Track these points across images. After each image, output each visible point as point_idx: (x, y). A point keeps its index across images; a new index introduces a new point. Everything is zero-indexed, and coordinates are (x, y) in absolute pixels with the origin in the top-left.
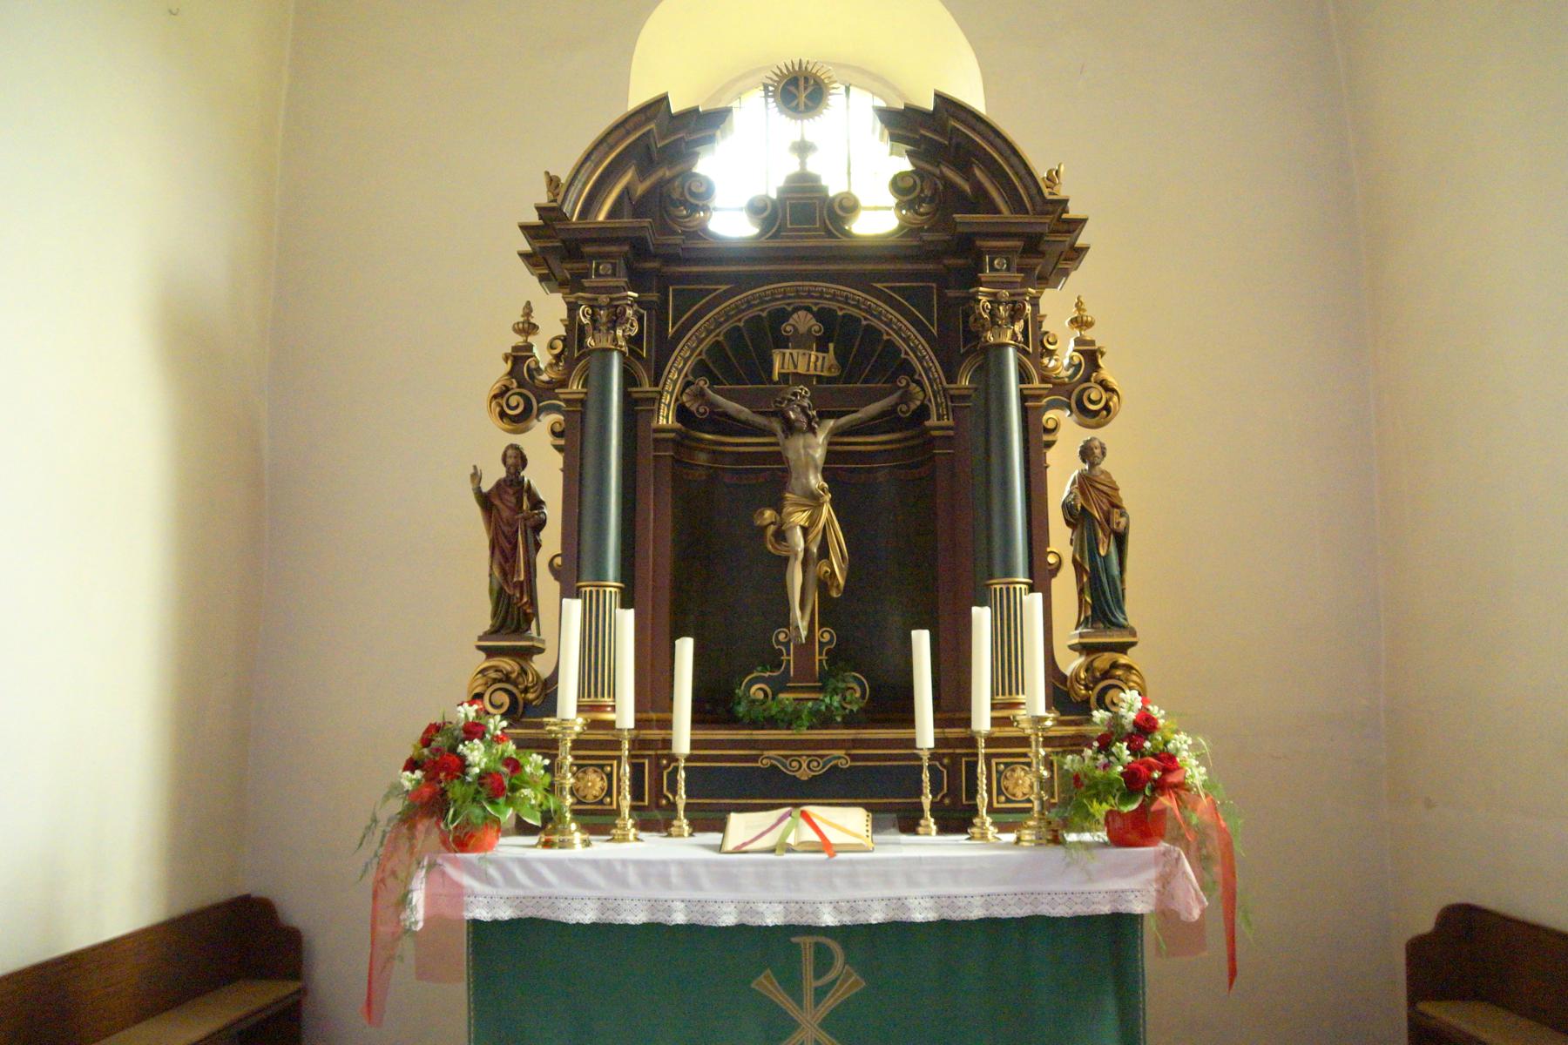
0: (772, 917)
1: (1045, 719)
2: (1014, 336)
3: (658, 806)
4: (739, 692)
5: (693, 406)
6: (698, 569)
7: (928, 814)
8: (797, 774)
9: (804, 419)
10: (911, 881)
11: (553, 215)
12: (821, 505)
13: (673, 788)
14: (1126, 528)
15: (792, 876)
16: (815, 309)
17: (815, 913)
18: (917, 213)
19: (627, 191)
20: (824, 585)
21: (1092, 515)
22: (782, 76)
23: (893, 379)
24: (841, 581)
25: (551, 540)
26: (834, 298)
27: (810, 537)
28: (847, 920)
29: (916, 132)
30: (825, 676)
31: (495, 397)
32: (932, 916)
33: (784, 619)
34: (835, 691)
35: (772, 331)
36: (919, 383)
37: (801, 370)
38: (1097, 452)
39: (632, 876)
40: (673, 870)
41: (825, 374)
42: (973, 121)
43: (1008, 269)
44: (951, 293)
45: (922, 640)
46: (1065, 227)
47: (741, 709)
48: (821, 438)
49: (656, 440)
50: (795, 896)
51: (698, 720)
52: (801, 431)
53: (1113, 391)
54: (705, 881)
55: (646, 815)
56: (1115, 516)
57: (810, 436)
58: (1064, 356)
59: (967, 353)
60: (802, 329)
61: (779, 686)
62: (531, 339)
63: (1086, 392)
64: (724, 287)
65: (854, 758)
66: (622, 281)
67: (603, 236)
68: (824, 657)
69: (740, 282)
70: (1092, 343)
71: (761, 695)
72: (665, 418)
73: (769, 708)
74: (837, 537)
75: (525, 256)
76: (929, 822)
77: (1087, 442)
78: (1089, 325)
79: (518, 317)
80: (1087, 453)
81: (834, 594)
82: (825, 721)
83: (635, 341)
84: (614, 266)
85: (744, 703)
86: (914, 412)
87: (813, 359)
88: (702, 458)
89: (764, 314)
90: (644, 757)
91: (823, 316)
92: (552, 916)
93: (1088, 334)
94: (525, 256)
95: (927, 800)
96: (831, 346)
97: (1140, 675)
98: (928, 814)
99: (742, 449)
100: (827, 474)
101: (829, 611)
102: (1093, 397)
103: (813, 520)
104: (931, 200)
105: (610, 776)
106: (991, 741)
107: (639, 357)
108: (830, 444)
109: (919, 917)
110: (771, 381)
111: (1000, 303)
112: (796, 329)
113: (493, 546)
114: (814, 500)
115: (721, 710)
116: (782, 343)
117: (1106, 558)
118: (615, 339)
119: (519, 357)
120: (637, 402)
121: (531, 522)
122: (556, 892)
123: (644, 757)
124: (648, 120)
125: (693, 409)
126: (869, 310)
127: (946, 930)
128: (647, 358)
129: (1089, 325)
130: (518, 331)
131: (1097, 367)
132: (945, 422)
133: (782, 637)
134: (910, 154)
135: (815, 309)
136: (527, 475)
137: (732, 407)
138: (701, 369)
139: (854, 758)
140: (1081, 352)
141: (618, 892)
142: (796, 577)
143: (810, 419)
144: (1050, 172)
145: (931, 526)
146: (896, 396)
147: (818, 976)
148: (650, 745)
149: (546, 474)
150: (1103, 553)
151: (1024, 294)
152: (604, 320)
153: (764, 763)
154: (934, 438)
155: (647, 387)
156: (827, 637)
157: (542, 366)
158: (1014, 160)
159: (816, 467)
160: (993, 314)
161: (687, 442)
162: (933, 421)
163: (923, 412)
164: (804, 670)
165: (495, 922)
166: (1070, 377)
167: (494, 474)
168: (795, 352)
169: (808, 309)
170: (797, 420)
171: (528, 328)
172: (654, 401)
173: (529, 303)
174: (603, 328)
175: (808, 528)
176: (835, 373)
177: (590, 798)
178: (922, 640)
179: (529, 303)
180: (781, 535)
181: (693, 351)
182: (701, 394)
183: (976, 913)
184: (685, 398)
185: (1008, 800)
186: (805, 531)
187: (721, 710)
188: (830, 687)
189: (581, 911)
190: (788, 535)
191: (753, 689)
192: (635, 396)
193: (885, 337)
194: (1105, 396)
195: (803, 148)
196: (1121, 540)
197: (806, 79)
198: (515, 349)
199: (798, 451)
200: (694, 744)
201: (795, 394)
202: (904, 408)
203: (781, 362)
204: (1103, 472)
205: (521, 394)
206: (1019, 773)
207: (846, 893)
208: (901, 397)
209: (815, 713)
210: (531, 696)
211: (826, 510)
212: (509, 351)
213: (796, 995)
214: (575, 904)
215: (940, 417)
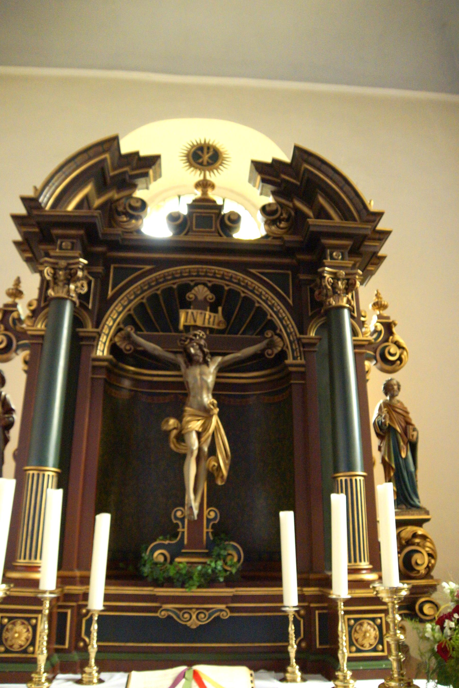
1: (401, 589)
2: (348, 301)
3: (77, 648)
4: (146, 555)
5: (123, 345)
7: (293, 661)
8: (188, 624)
9: (201, 354)
11: (33, 204)
12: (211, 416)
13: (88, 633)
14: (417, 438)
16: (209, 284)
18: (278, 227)
19: (86, 198)
20: (211, 476)
21: (395, 430)
23: (262, 333)
24: (225, 472)
26: (223, 278)
27: (203, 439)
29: (278, 176)
30: (210, 545)
33: (181, 501)
34: (219, 557)
35: (179, 297)
36: (280, 336)
37: (199, 323)
38: (396, 387)
41: (215, 327)
42: (319, 163)
43: (343, 259)
44: (302, 277)
45: (287, 519)
46: (377, 236)
47: (146, 570)
48: (212, 368)
49: (94, 367)
51: (114, 574)
52: (198, 363)
55: (66, 657)
56: (410, 432)
57: (204, 367)
58: (372, 323)
59: (313, 317)
60: (200, 298)
61: (176, 552)
62: (17, 300)
63: (383, 351)
65: (232, 610)
66: (77, 253)
67: (68, 222)
68: (210, 530)
69: (160, 264)
70: (388, 318)
71: (161, 559)
72: (102, 350)
73: (168, 570)
74: (223, 440)
75: (17, 244)
76: (294, 669)
78: (384, 307)
79: (10, 285)
80: (389, 389)
82: (210, 581)
83: (84, 298)
84: (73, 243)
85: (148, 566)
86: (276, 355)
87: (207, 317)
88: (127, 383)
89: (175, 286)
90: (68, 607)
91: (215, 289)
93: (385, 313)
94: (17, 244)
95: (292, 650)
96: (220, 309)
97: (431, 542)
98: (293, 661)
99: (155, 379)
101: (215, 495)
102: (392, 351)
103: (205, 427)
104: (287, 220)
105: (35, 628)
106: (347, 602)
107: (86, 309)
108: (217, 377)
110: (176, 329)
111: (339, 279)
112: (196, 297)
114: (206, 413)
115: (131, 568)
116: (186, 305)
117: (406, 459)
118: (69, 291)
120: (82, 338)
121: (3, 423)
123: (68, 607)
124: (104, 152)
125: (122, 347)
126: (246, 287)
128: (90, 311)
129: (384, 307)
130: (10, 294)
131: (391, 333)
132: (299, 361)
133: (179, 514)
134: (274, 193)
135: (209, 284)
137: (150, 346)
138: (129, 320)
139: (232, 610)
140: (382, 323)
142: (192, 469)
143: (205, 354)
145: (294, 431)
148: (71, 599)
150: (403, 455)
151: (356, 274)
152: (62, 278)
153: (162, 614)
154: (291, 373)
155: (90, 328)
156: (212, 515)
157: (23, 317)
158: (347, 188)
159: (208, 389)
160: (334, 286)
161: (116, 371)
162: (290, 361)
163: (282, 355)
164: (195, 539)
166: (376, 339)
168: (195, 312)
169: (205, 284)
170: (196, 355)
171: (16, 293)
172: (95, 339)
174: (61, 284)
175: (201, 432)
176: (222, 327)
177: (16, 647)
178: (287, 519)
180: (181, 437)
181: (124, 307)
182: (128, 337)
184: (116, 339)
185: (358, 651)
186: (199, 435)
187: (131, 568)
188: (215, 553)
190: (186, 437)
191: (156, 554)
192: (82, 334)
193: (257, 305)
194: (398, 352)
195: (204, 185)
196: (413, 447)
198: (6, 305)
199: (195, 377)
200: (107, 597)
201: (195, 335)
202: (270, 351)
203: (184, 318)
204: (398, 401)
206: (366, 627)
208: (268, 344)
209: (203, 575)
211: (215, 420)
215: (295, 358)
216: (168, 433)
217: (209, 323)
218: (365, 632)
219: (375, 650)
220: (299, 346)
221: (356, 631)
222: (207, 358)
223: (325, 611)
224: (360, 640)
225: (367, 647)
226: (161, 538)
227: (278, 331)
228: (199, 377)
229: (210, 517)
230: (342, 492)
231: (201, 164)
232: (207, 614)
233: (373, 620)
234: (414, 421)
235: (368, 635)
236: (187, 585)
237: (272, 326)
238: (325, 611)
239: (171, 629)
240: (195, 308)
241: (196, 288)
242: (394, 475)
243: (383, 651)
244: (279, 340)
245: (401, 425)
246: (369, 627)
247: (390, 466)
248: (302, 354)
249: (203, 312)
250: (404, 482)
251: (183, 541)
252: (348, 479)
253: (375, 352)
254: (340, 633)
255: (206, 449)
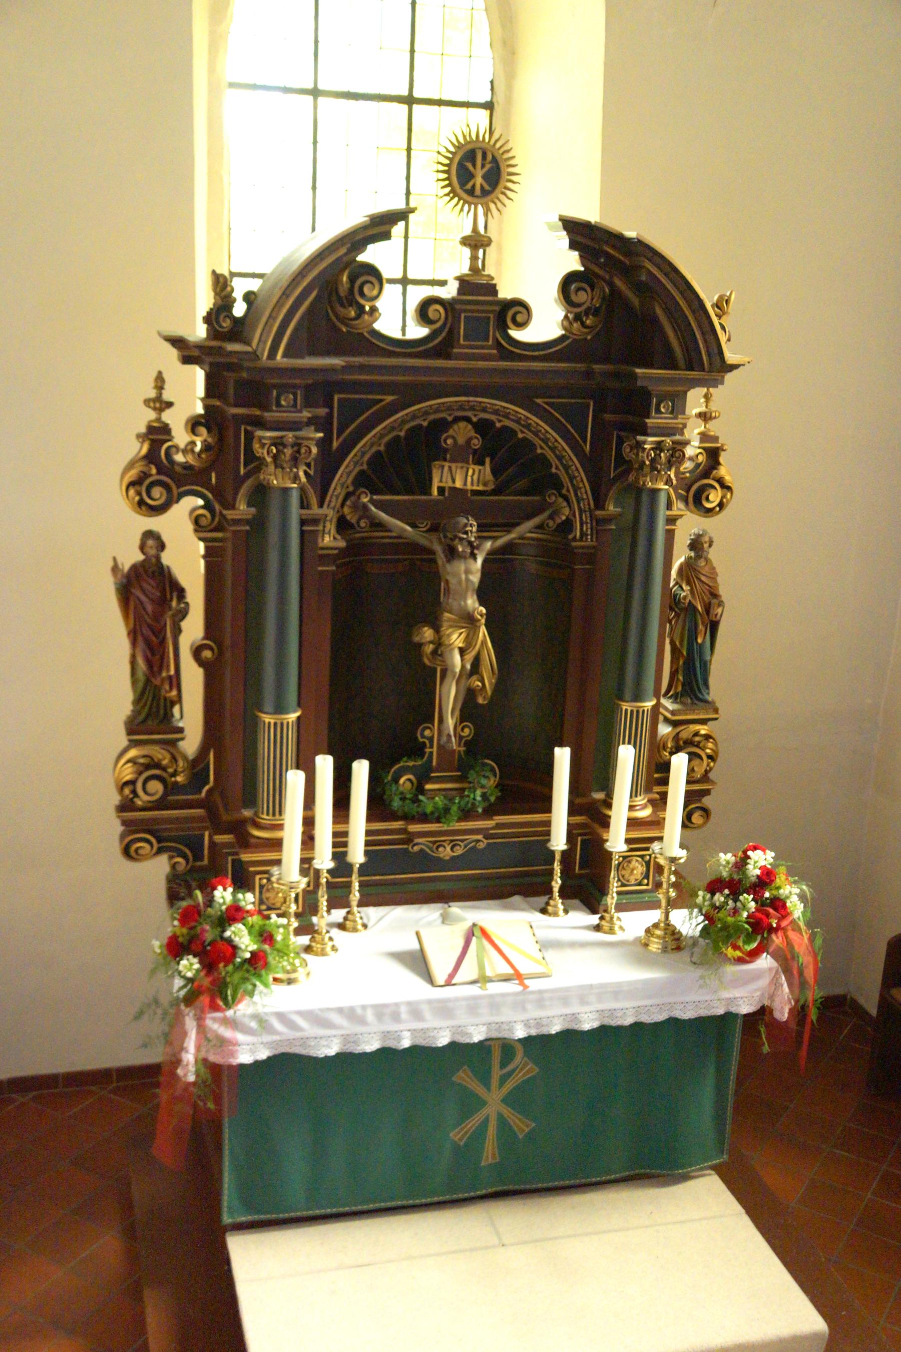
0: (477, 1036)
5: (351, 518)
6: (371, 717)
10: (583, 1001)
15: (494, 1003)
16: (475, 419)
17: (511, 1030)
20: (471, 694)
21: (695, 609)
22: (459, 147)
24: (489, 692)
25: (193, 628)
28: (533, 1032)
31: (132, 484)
32: (596, 1025)
38: (706, 546)
39: (370, 1016)
40: (403, 1009)
41: (481, 488)
45: (563, 756)
49: (321, 556)
50: (498, 1019)
53: (729, 488)
54: (428, 1015)
57: (471, 561)
63: (703, 485)
64: (389, 398)
70: (715, 439)
77: (699, 536)
81: (480, 701)
92: (303, 1052)
97: (716, 744)
100: (483, 595)
101: (469, 709)
109: (586, 1027)
113: (134, 635)
114: (469, 620)
117: (701, 646)
119: (157, 434)
122: (306, 1034)
127: (605, 1033)
135: (475, 419)
136: (167, 558)
141: (359, 1029)
144: (721, 297)
146: (546, 514)
147: (503, 1065)
149: (187, 560)
150: (700, 641)
165: (257, 1063)
167: (131, 557)
169: (468, 419)
171: (161, 404)
173: (160, 373)
175: (462, 647)
178: (563, 756)
179: (160, 373)
183: (628, 1021)
186: (462, 651)
189: (328, 1046)
196: (714, 627)
197: (484, 155)
199: (457, 575)
205: (156, 477)
206: (634, 864)
207: (534, 1013)
210: (179, 779)
211: (483, 630)
212: (143, 430)
213: (487, 1083)
214: (323, 1042)
216: (420, 645)
217: (472, 484)
218: (632, 870)
219: (640, 884)
220: (591, 520)
221: (623, 868)
222: (349, 286)
223: (588, 837)
224: (626, 876)
225: (633, 882)
226: (405, 759)
227: (564, 491)
228: (463, 577)
229: (463, 734)
230: (629, 743)
231: (471, 192)
232: (462, 844)
233: (642, 857)
234: (722, 591)
235: (635, 872)
236: (443, 820)
237: (556, 484)
238: (588, 837)
239: (426, 861)
240: (453, 461)
241: (455, 427)
242: (684, 663)
243: (647, 885)
244: (565, 504)
245: (703, 600)
246: (637, 864)
247: (680, 652)
248: (595, 532)
249: (466, 465)
250: (695, 675)
251: (431, 762)
252: (635, 710)
253: (688, 491)
254: (611, 880)
255: (468, 667)
